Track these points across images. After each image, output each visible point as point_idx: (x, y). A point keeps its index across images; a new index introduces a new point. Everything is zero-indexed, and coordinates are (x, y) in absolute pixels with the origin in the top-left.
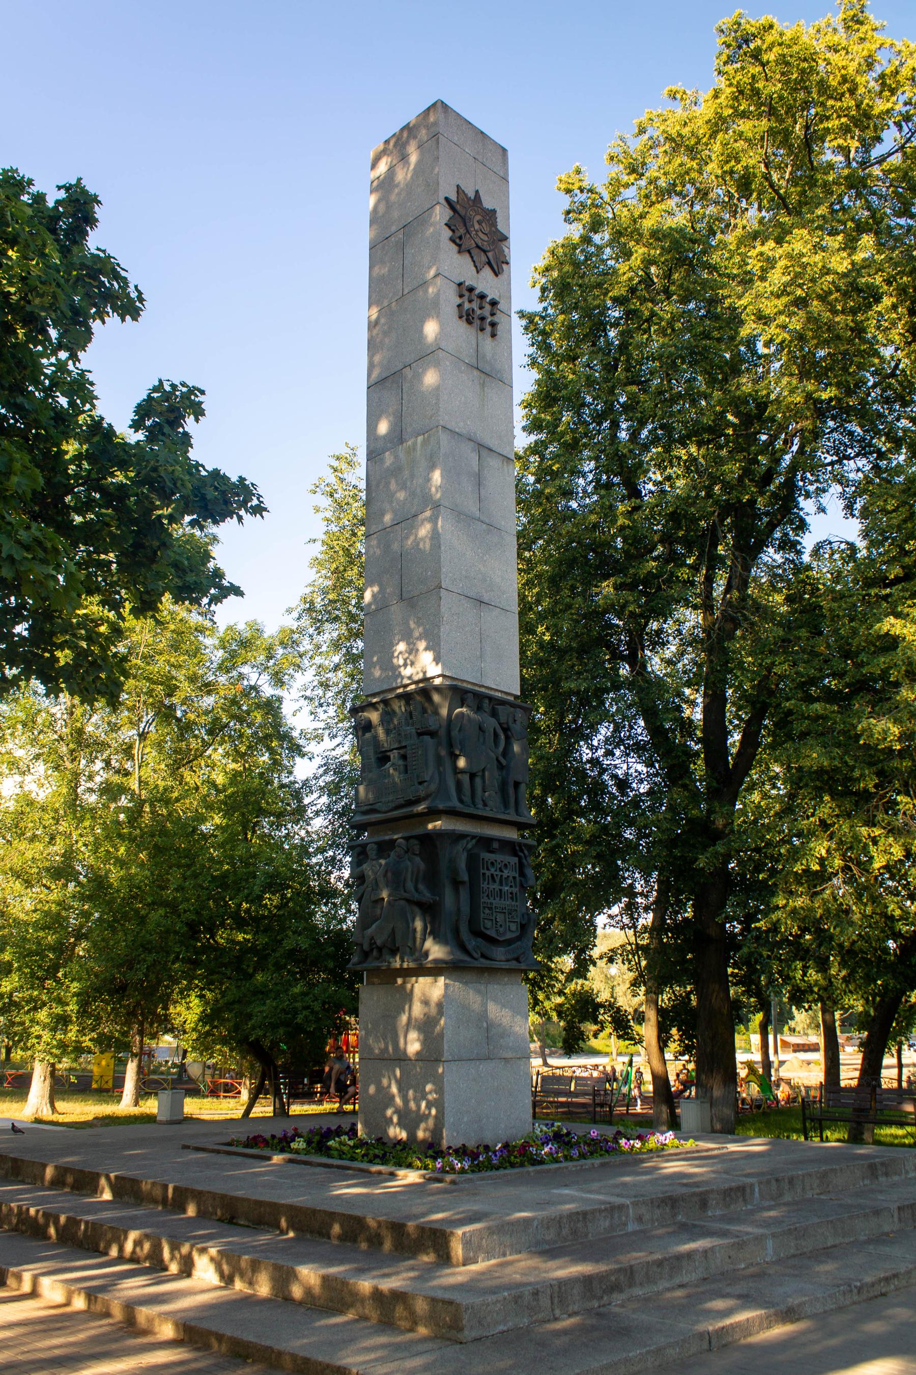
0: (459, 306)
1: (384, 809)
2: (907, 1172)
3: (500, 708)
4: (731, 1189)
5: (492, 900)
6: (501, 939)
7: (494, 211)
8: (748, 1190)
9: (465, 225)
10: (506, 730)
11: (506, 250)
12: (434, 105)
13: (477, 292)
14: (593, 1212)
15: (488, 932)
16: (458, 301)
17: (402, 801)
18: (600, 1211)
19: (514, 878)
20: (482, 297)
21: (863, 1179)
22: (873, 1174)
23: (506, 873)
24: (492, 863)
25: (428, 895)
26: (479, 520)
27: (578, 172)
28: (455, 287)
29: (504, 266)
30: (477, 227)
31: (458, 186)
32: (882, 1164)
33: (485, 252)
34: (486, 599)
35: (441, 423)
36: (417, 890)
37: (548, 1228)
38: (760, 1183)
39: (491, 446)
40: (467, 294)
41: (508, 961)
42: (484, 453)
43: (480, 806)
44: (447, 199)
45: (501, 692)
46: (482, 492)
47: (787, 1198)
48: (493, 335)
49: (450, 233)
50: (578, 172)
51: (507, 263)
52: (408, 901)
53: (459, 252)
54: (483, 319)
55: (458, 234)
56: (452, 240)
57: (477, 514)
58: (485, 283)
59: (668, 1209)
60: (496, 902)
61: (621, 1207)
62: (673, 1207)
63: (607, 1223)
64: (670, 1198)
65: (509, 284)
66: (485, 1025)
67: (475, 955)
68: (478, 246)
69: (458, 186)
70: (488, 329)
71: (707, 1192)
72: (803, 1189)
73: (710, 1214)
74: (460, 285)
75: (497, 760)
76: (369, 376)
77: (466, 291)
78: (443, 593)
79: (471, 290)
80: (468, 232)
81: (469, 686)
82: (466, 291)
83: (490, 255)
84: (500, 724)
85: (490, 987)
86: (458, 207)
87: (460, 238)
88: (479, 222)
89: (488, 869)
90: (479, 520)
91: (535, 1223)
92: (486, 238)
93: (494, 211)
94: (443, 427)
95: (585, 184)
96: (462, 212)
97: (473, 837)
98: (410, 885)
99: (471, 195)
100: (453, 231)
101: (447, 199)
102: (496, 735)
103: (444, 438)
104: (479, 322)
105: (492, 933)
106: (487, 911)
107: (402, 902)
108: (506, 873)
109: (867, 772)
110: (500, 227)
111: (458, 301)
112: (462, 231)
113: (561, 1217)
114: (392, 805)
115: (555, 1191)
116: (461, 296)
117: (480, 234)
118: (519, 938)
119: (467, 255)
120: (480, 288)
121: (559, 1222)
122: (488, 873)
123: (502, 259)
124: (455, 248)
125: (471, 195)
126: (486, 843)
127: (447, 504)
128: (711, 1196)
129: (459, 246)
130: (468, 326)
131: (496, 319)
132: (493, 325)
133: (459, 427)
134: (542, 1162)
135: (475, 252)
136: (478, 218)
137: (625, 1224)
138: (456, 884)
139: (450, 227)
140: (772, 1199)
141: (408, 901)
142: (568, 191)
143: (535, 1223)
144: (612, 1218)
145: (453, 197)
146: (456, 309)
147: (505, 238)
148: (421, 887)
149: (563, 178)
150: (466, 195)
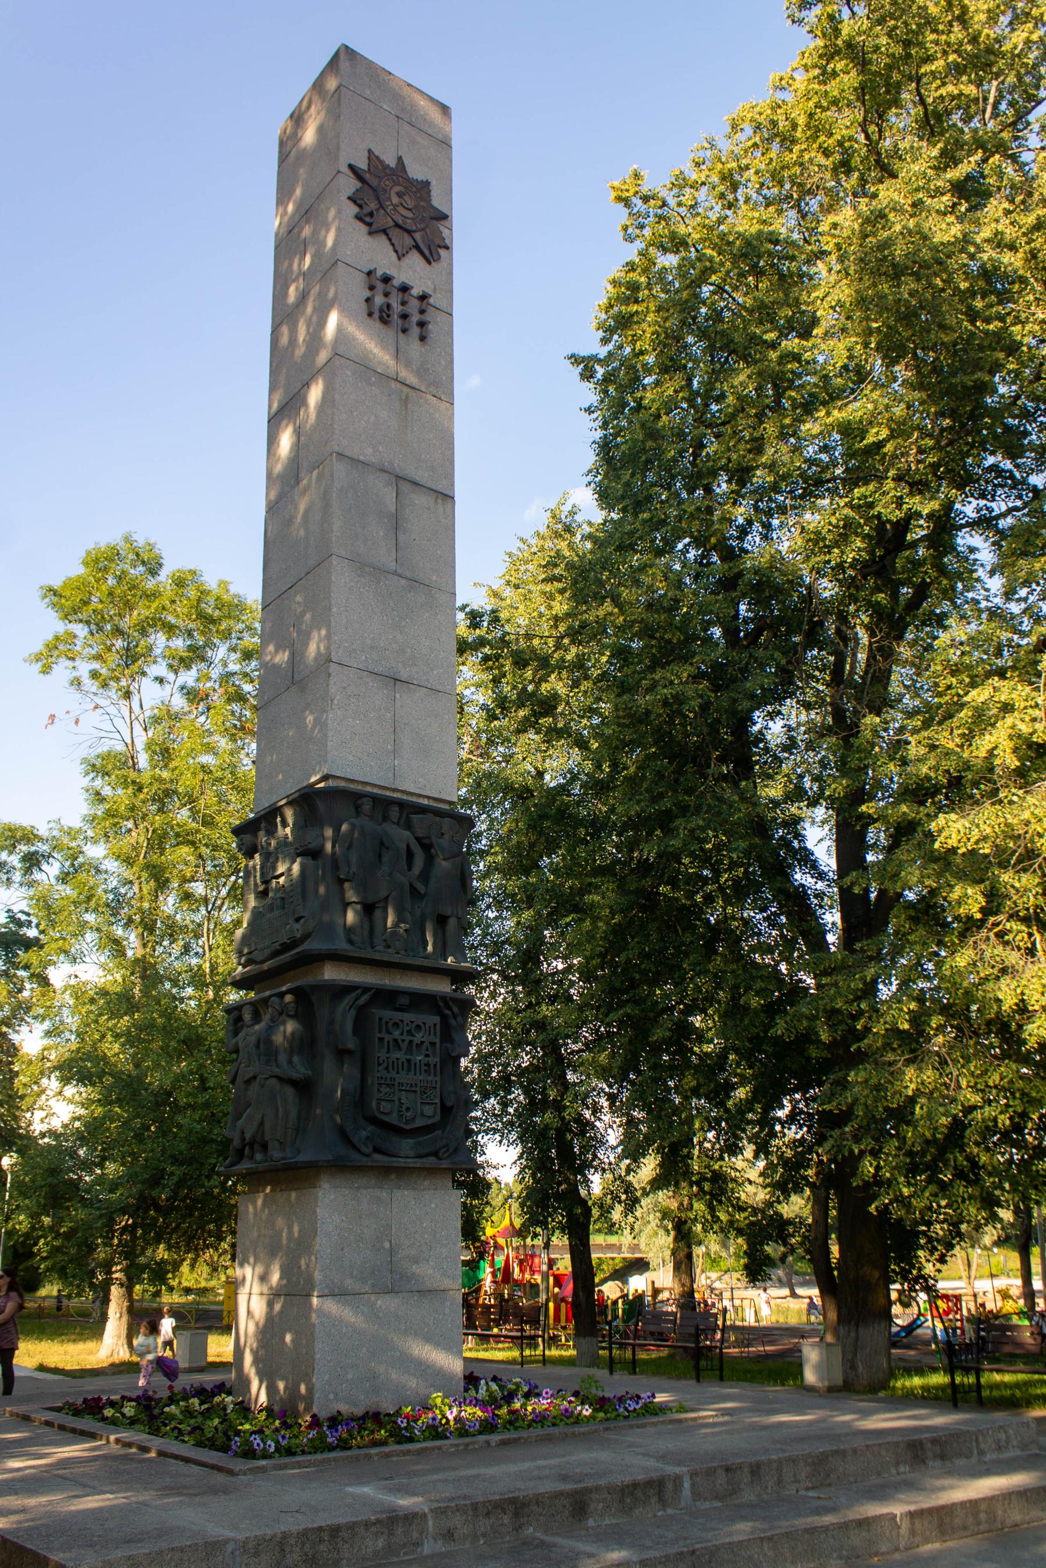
0: (367, 300)
1: (260, 958)
2: (982, 1453)
3: (415, 818)
4: (635, 1485)
5: (394, 1074)
6: (408, 1127)
7: (427, 184)
8: (670, 1486)
9: (378, 199)
10: (427, 847)
11: (445, 233)
12: (337, 55)
13: (415, 292)
14: (352, 1526)
15: (386, 1118)
16: (367, 294)
17: (277, 946)
18: (367, 1524)
19: (433, 1044)
20: (405, 289)
21: (897, 1464)
22: (916, 1457)
23: (418, 1037)
24: (396, 1025)
25: (302, 1070)
26: (395, 573)
27: (637, 176)
28: (363, 277)
29: (443, 252)
30: (395, 200)
31: (370, 151)
32: (934, 1441)
33: (409, 232)
34: (404, 675)
35: (336, 448)
36: (290, 1062)
37: (257, 1554)
38: (693, 1474)
39: (418, 479)
40: (380, 286)
41: (420, 1156)
42: (406, 487)
43: (381, 948)
44: (351, 167)
45: (429, 798)
46: (402, 538)
47: (748, 1496)
48: (422, 338)
49: (355, 210)
50: (637, 176)
51: (447, 248)
52: (280, 1079)
53: (370, 233)
54: (404, 316)
55: (367, 210)
56: (359, 218)
57: (393, 566)
58: (412, 271)
59: (506, 1520)
60: (403, 1077)
61: (410, 1518)
62: (516, 1515)
63: (381, 1543)
64: (512, 1501)
65: (451, 273)
66: (387, 1245)
67: (364, 1149)
68: (397, 225)
69: (370, 151)
70: (415, 331)
71: (587, 1491)
72: (779, 1482)
73: (591, 1522)
74: (369, 273)
75: (411, 885)
76: (270, 407)
77: (378, 281)
78: (333, 668)
79: (387, 279)
80: (381, 206)
81: (426, 802)
82: (378, 281)
83: (418, 236)
84: (417, 839)
85: (397, 1193)
86: (367, 177)
87: (371, 214)
88: (400, 195)
89: (390, 1033)
90: (395, 573)
91: (230, 1547)
92: (410, 215)
93: (427, 184)
94: (339, 454)
95: (645, 190)
96: (374, 182)
97: (366, 989)
98: (282, 1058)
99: (392, 163)
100: (360, 206)
101: (351, 167)
102: (410, 855)
103: (340, 468)
104: (400, 321)
105: (393, 1119)
106: (385, 1089)
107: (273, 1081)
108: (418, 1037)
109: (970, 891)
110: (437, 201)
111: (367, 294)
112: (373, 206)
113: (285, 1536)
114: (267, 952)
115: (350, 1489)
116: (372, 288)
117: (401, 209)
118: (441, 1125)
119: (384, 238)
120: (401, 277)
121: (281, 1544)
122: (387, 1037)
123: (438, 241)
124: (364, 228)
125: (392, 163)
126: (388, 997)
127: (343, 553)
128: (594, 1496)
129: (369, 225)
130: (382, 326)
131: (427, 317)
132: (422, 324)
133: (368, 454)
134: (411, 1440)
135: (394, 233)
136: (397, 189)
137: (418, 1544)
138: (342, 1053)
139: (355, 202)
140: (717, 1498)
141: (280, 1079)
142: (626, 202)
143: (230, 1547)
144: (391, 1534)
145: (362, 164)
146: (364, 305)
147: (444, 217)
148: (296, 1059)
149: (616, 184)
150: (381, 162)
